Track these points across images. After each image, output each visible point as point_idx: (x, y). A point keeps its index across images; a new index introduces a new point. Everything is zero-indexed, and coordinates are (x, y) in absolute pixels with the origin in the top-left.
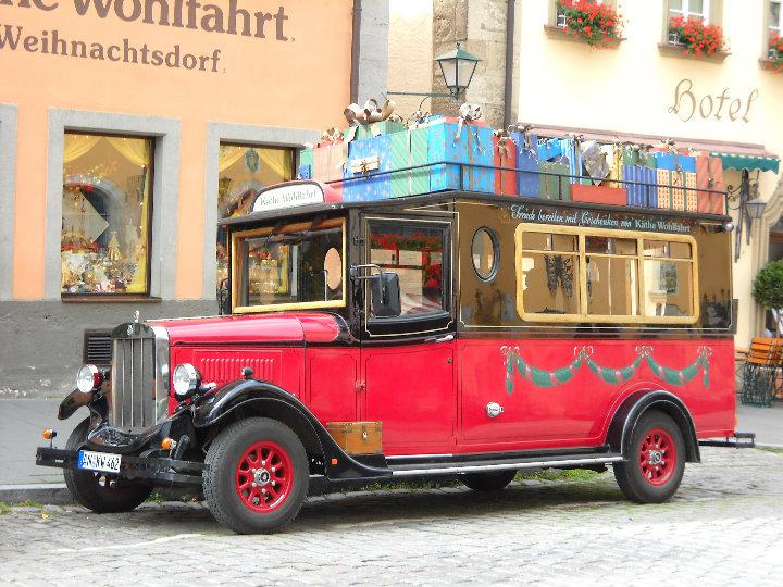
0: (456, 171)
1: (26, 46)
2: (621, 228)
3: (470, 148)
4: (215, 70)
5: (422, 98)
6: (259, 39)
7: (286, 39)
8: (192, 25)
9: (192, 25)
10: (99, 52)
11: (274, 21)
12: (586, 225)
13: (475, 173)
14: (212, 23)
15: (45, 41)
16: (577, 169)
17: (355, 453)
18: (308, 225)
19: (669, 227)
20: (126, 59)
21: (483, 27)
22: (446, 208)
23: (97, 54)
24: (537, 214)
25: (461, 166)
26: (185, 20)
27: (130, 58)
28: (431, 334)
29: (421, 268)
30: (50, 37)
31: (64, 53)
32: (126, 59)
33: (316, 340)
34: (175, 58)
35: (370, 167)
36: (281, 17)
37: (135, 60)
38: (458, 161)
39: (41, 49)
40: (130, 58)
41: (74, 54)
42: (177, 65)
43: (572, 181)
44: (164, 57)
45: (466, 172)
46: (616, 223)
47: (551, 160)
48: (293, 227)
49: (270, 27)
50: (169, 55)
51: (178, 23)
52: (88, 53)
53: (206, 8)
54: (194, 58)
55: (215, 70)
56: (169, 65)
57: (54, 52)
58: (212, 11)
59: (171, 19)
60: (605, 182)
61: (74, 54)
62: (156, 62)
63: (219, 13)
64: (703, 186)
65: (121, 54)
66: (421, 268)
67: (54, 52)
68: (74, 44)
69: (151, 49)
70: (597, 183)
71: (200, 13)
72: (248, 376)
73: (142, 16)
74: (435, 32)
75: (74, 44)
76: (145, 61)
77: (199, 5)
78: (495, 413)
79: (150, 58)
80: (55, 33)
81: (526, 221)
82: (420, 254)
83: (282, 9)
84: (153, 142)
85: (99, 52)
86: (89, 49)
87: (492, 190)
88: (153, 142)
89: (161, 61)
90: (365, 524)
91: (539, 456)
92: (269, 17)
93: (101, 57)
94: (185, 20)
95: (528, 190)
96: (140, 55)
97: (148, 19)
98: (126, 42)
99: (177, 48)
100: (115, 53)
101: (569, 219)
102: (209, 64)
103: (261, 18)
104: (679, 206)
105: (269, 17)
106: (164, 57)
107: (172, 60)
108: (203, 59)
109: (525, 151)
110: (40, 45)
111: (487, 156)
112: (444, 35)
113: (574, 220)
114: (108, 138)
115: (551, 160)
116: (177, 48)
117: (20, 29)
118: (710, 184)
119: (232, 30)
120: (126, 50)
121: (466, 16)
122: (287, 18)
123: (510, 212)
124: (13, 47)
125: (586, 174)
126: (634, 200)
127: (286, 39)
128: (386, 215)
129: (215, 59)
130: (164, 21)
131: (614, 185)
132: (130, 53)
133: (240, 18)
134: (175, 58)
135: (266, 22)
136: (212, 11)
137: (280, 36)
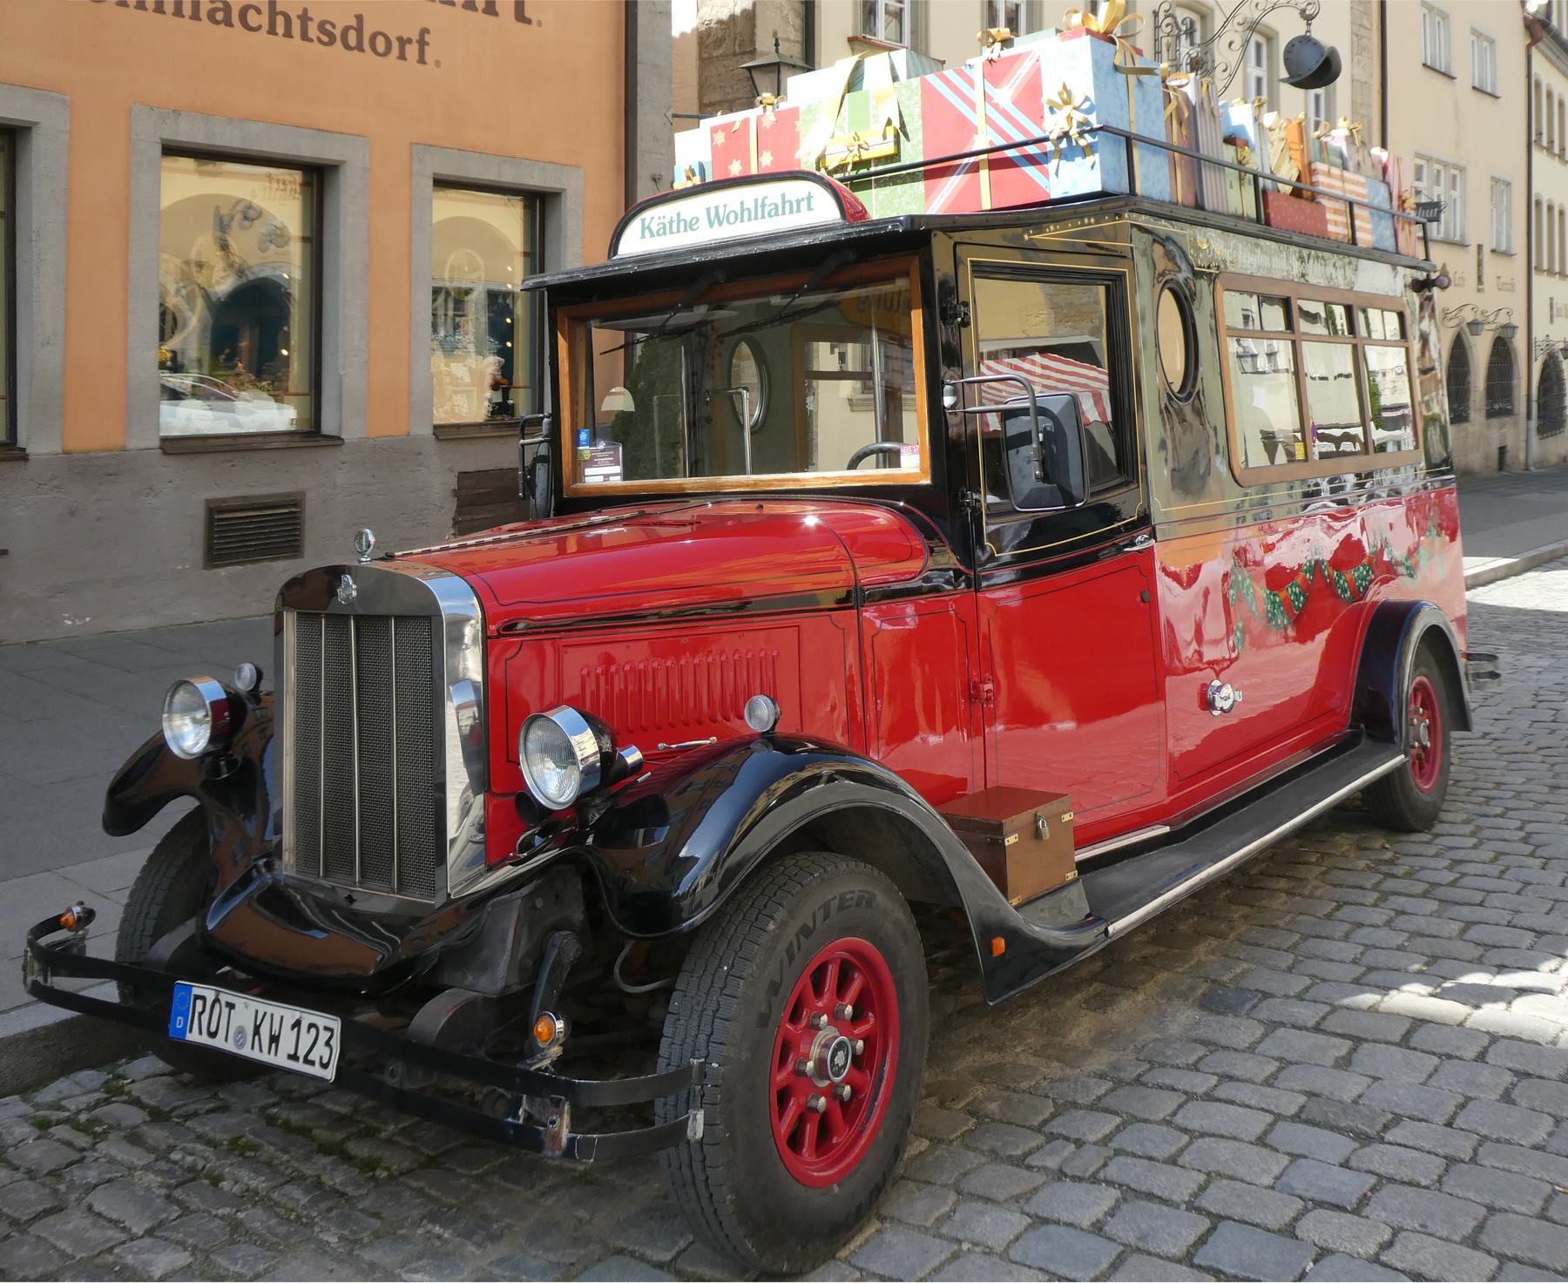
4: (422, 60)
6: (489, 18)
7: (529, 22)
20: (272, 31)
23: (220, 16)
27: (280, 29)
39: (266, 27)
40: (280, 29)
42: (360, 48)
44: (337, 33)
49: (804, 205)
55: (422, 60)
56: (347, 46)
62: (325, 39)
65: (264, 20)
69: (317, 16)
71: (767, 209)
76: (305, 37)
79: (313, 31)
99: (359, 18)
100: (252, 18)
102: (412, 51)
106: (337, 33)
107: (352, 38)
108: (403, 42)
116: (359, 18)
124: (720, 224)
127: (529, 22)
129: (422, 43)
132: (280, 20)
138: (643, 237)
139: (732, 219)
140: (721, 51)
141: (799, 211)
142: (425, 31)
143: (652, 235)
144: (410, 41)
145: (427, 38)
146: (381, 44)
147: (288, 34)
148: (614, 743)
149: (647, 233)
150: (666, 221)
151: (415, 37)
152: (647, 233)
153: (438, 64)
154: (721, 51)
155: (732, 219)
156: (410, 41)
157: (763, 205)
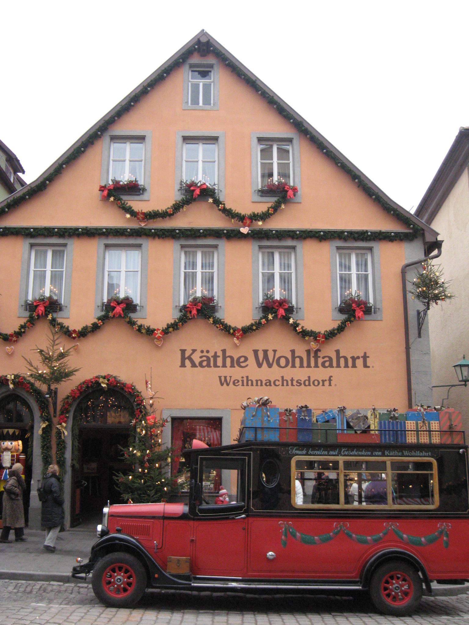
2: (330, 455)
5: (449, 387)
6: (354, 369)
7: (369, 367)
8: (316, 366)
9: (316, 366)
11: (361, 359)
14: (327, 364)
15: (243, 381)
17: (174, 572)
19: (413, 453)
20: (283, 385)
23: (268, 384)
24: (328, 452)
27: (285, 384)
29: (315, 479)
30: (245, 379)
31: (252, 385)
32: (283, 385)
33: (269, 519)
34: (308, 382)
36: (365, 357)
39: (281, 384)
40: (285, 384)
42: (309, 385)
44: (302, 382)
49: (360, 362)
50: (305, 382)
51: (309, 366)
53: (323, 358)
54: (318, 381)
55: (330, 385)
56: (305, 385)
58: (327, 359)
60: (367, 431)
61: (257, 385)
62: (298, 384)
63: (331, 359)
64: (446, 428)
65: (280, 383)
66: (315, 479)
67: (247, 385)
68: (257, 381)
69: (296, 379)
73: (290, 365)
75: (257, 381)
76: (292, 385)
77: (320, 357)
78: (271, 557)
79: (295, 383)
80: (247, 377)
82: (236, 471)
86: (264, 382)
87: (277, 439)
89: (301, 384)
90: (201, 611)
91: (335, 583)
92: (358, 358)
94: (313, 364)
97: (293, 366)
98: (283, 377)
99: (309, 377)
100: (277, 383)
102: (327, 383)
103: (354, 359)
104: (424, 439)
106: (302, 382)
107: (307, 383)
108: (323, 381)
110: (240, 383)
113: (336, 453)
116: (309, 377)
117: (231, 377)
118: (451, 427)
119: (338, 366)
120: (283, 380)
122: (368, 357)
123: (288, 450)
124: (228, 385)
126: (389, 440)
127: (369, 367)
129: (330, 380)
131: (373, 432)
132: (285, 382)
135: (357, 361)
136: (327, 359)
137: (365, 366)
138: (183, 365)
139: (283, 362)
143: (194, 365)
145: (332, 378)
146: (316, 383)
149: (187, 362)
150: (210, 355)
151: (327, 379)
152: (187, 362)
155: (283, 362)
156: (326, 380)
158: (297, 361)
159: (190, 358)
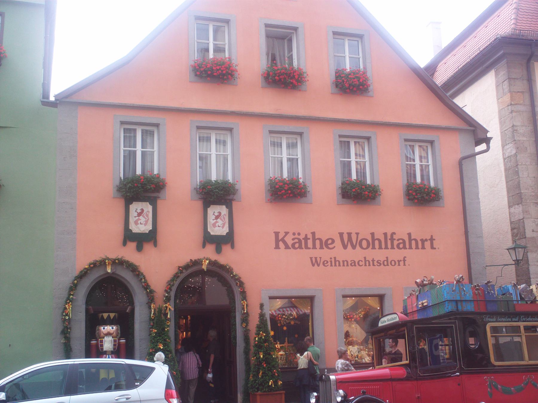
0: (454, 303)
1: (324, 264)
3: (461, 293)
4: (404, 265)
7: (435, 249)
8: (393, 248)
10: (354, 264)
11: (429, 242)
12: (524, 321)
13: (464, 303)
14: (401, 246)
15: (331, 261)
16: (517, 296)
18: (394, 331)
20: (366, 265)
21: (533, 231)
22: (450, 319)
23: (353, 264)
25: (457, 301)
26: (389, 246)
27: (367, 264)
28: (450, 373)
30: (333, 260)
31: (339, 265)
32: (366, 265)
34: (387, 262)
35: (425, 304)
36: (432, 240)
37: (369, 265)
38: (455, 299)
40: (367, 264)
41: (344, 265)
42: (388, 265)
43: (515, 302)
44: (382, 262)
45: (459, 304)
46: (510, 320)
47: (504, 294)
48: (390, 332)
49: (427, 244)
51: (386, 248)
52: (349, 264)
53: (398, 240)
54: (395, 261)
55: (404, 265)
56: (384, 265)
57: (335, 265)
58: (401, 241)
59: (383, 246)
61: (344, 265)
65: (363, 263)
67: (335, 265)
68: (343, 261)
69: (376, 260)
70: (529, 302)
71: (396, 243)
72: (364, 393)
73: (371, 246)
74: (512, 236)
75: (343, 261)
76: (374, 265)
79: (375, 263)
80: (335, 258)
81: (490, 322)
83: (432, 236)
84: (381, 298)
85: (354, 264)
86: (350, 263)
87: (473, 310)
88: (381, 298)
92: (426, 240)
93: (355, 265)
94: (389, 246)
95: (491, 308)
96: (371, 263)
97: (374, 248)
98: (365, 258)
99: (387, 258)
100: (361, 263)
101: (514, 319)
103: (423, 241)
105: (426, 240)
106: (382, 262)
108: (399, 261)
109: (488, 292)
111: (469, 296)
112: (516, 236)
114: (362, 298)
115: (504, 294)
116: (387, 258)
117: (320, 258)
119: (410, 248)
120: (365, 261)
121: (524, 227)
124: (318, 265)
125: (522, 299)
127: (435, 249)
128: (423, 324)
129: (404, 260)
130: (380, 248)
133: (413, 242)
134: (387, 262)
137: (432, 247)
139: (364, 244)
140: (517, 238)
141: (423, 248)
142: (405, 257)
143: (287, 247)
144: (401, 261)
147: (369, 265)
148: (517, 283)
149: (281, 244)
150: (302, 237)
151: (402, 259)
152: (281, 244)
153: (409, 265)
154: (517, 238)
155: (364, 244)
156: (401, 261)
157: (392, 239)
158: (377, 242)
159: (283, 240)
